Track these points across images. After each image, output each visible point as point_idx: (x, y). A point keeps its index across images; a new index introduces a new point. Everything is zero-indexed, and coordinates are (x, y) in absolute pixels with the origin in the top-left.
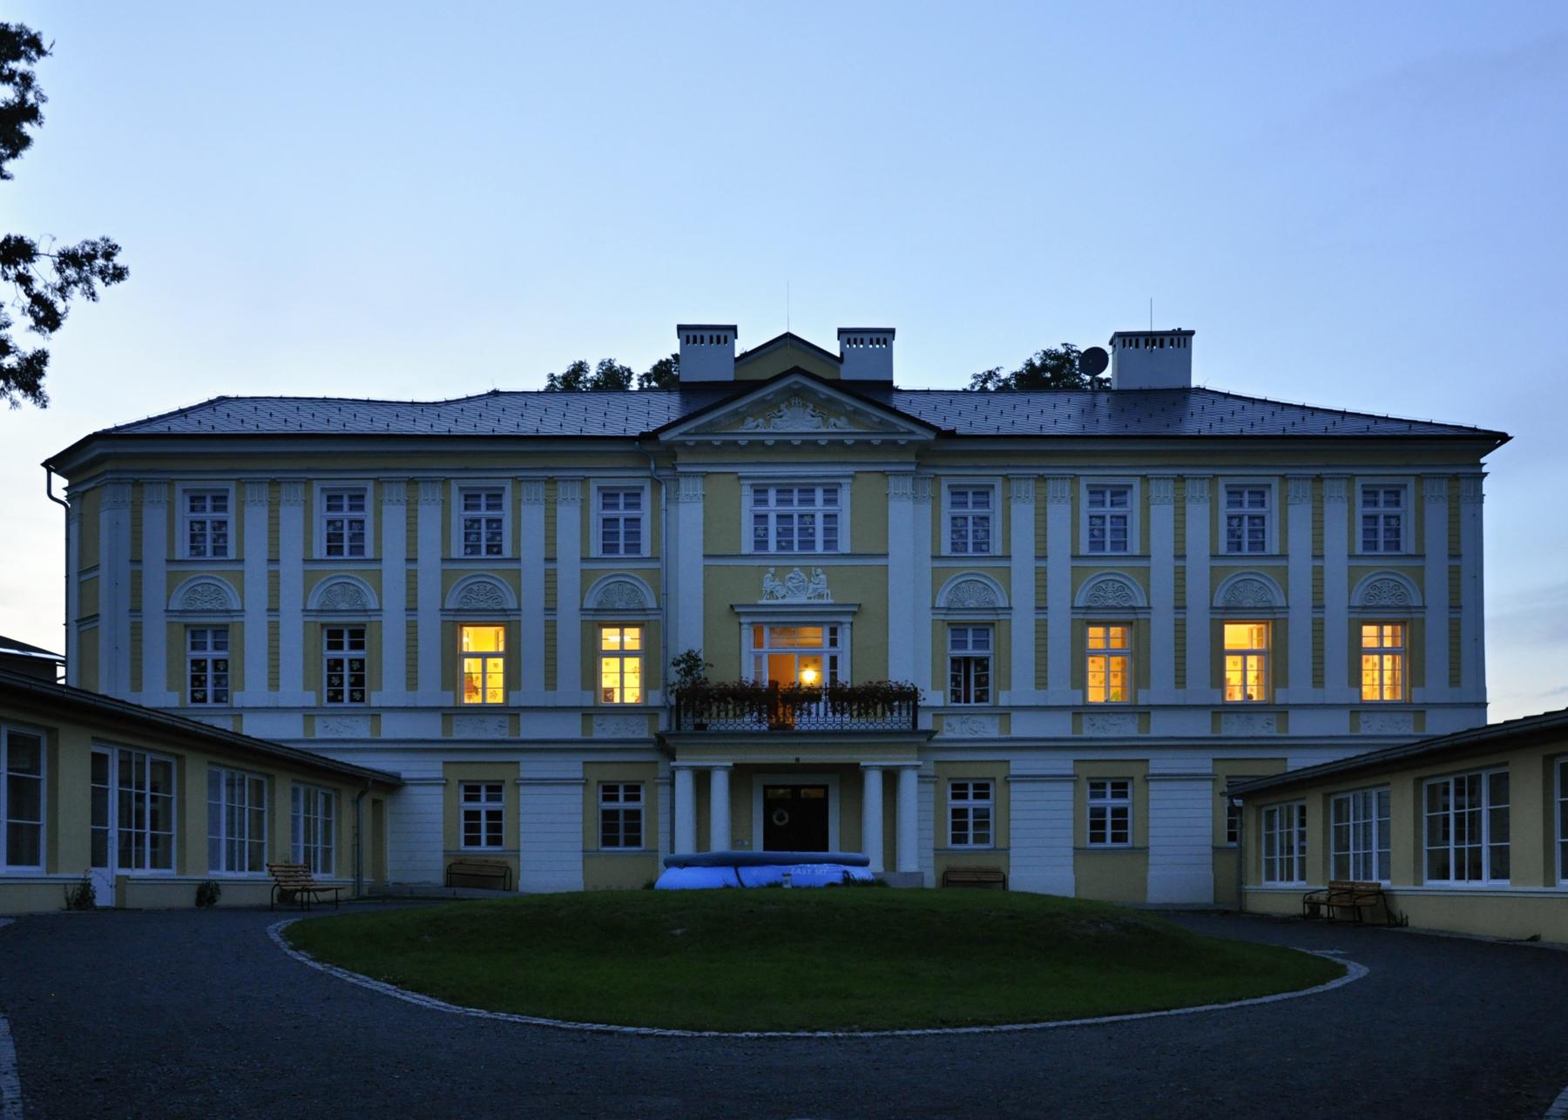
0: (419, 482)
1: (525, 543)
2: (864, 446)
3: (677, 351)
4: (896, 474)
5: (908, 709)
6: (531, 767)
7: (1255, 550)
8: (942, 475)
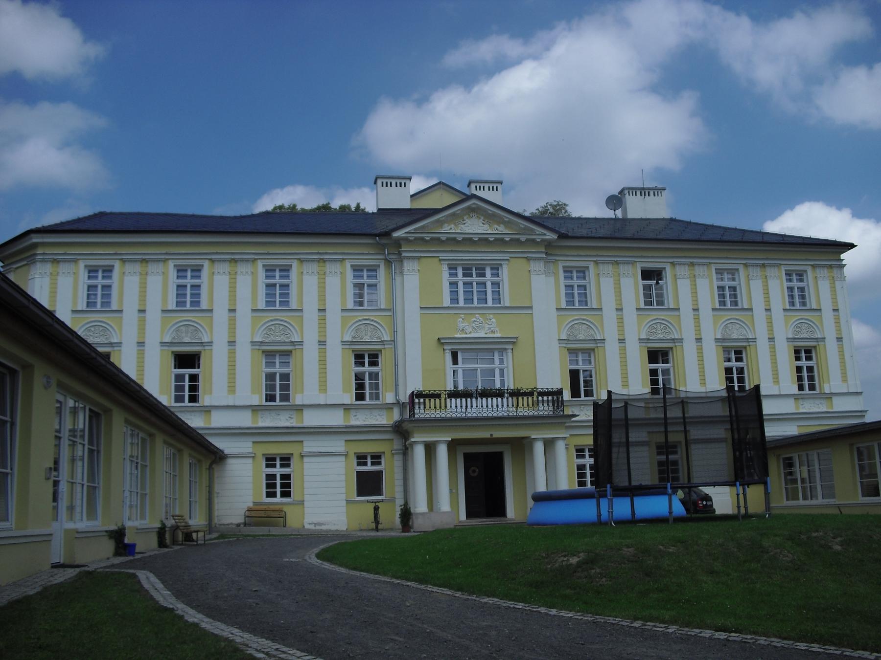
0: (238, 261)
2: (516, 242)
4: (535, 259)
6: (311, 445)
7: (582, 305)
8: (559, 260)
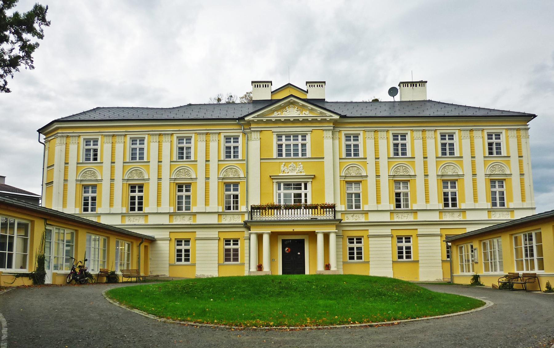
1: (199, 154)
3: (252, 90)
5: (332, 212)
